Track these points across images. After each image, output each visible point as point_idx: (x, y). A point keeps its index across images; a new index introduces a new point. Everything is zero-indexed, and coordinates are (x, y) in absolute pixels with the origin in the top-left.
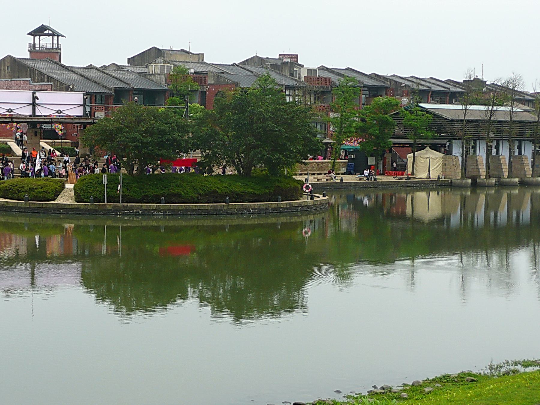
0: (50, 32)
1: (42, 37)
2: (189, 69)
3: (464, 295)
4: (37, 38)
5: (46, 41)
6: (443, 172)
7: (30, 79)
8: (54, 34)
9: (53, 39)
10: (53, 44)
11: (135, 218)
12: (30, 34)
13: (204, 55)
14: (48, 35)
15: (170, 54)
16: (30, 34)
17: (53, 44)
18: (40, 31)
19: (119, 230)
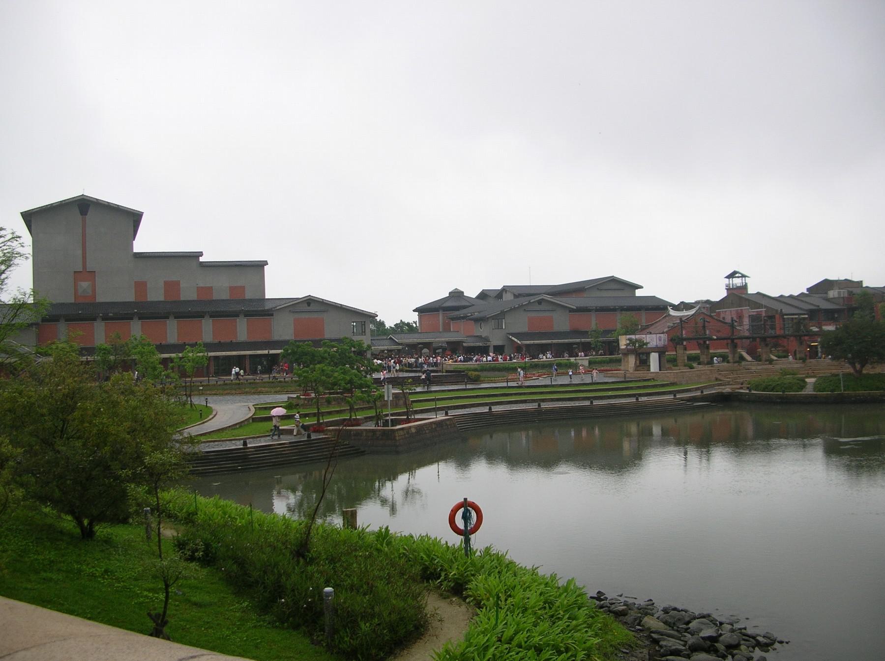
0: (740, 275)
1: (734, 279)
2: (421, 376)
3: (686, 466)
4: (731, 279)
5: (737, 282)
6: (135, 299)
7: (748, 308)
8: (743, 276)
9: (742, 279)
10: (742, 283)
11: (773, 333)
12: (726, 277)
13: (22, 212)
14: (738, 277)
15: (56, 348)
16: (726, 277)
17: (742, 283)
18: (732, 275)
19: (856, 437)
